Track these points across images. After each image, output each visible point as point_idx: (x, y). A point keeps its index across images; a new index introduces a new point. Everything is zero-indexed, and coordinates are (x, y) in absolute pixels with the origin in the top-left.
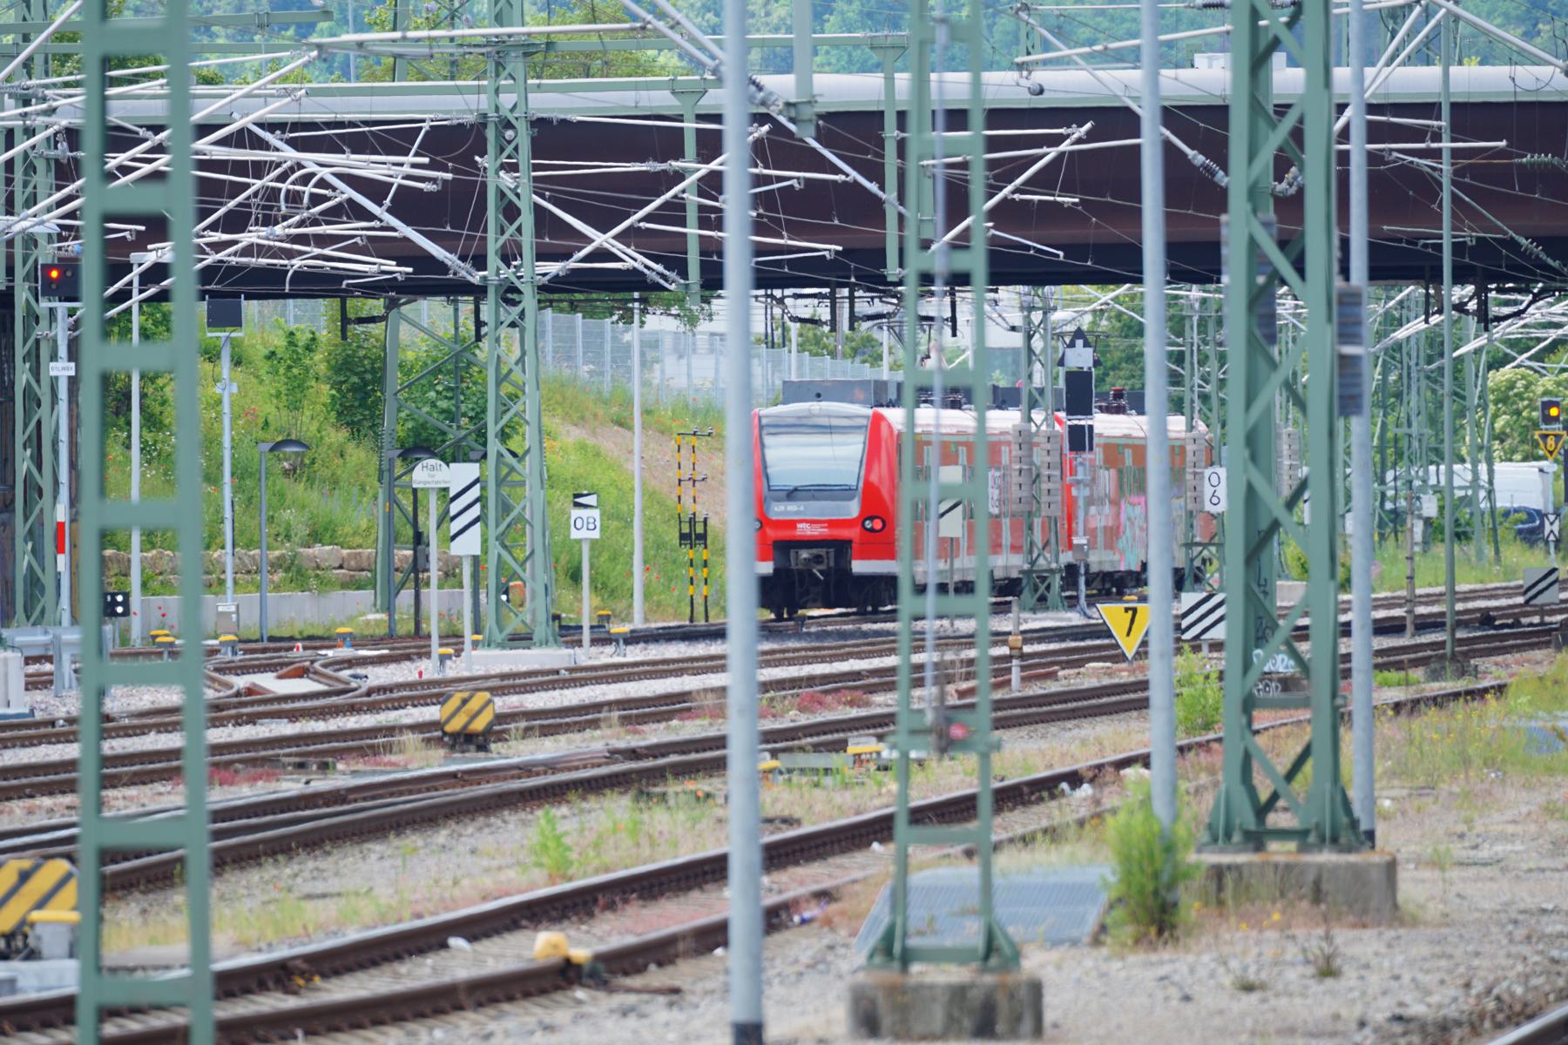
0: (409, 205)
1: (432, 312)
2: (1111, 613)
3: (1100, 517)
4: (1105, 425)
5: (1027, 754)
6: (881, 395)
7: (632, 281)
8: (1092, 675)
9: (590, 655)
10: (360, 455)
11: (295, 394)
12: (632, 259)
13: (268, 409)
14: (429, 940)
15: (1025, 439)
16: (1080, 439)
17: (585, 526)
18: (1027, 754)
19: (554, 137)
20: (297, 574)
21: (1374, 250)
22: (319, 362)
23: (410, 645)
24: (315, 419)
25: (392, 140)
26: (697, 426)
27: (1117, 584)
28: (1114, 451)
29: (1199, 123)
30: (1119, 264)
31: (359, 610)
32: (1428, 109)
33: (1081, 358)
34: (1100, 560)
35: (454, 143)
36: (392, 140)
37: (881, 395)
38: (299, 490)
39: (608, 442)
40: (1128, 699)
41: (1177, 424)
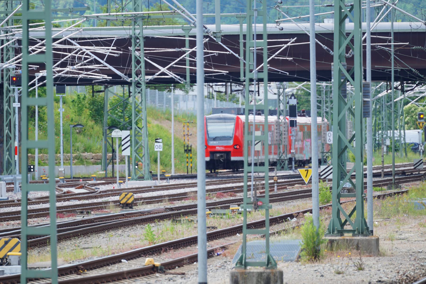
0: (111, 60)
1: (117, 89)
2: (301, 171)
3: (298, 145)
4: (300, 120)
5: (279, 209)
6: (239, 112)
7: (171, 81)
8: (297, 188)
9: (159, 183)
10: (98, 128)
11: (80, 111)
12: (171, 75)
13: (73, 116)
14: (116, 260)
15: (278, 124)
16: (293, 124)
17: (158, 147)
18: (279, 209)
19: (150, 42)
20: (81, 161)
21: (373, 72)
22: (86, 103)
23: (111, 180)
24: (85, 118)
25: (106, 43)
26: (189, 120)
27: (303, 163)
28: (302, 127)
29: (326, 38)
30: (304, 76)
31: (97, 171)
32: (387, 34)
33: (293, 102)
34: (299, 157)
35: (123, 43)
36: (106, 43)
37: (239, 112)
38: (81, 137)
39: (165, 125)
40: (306, 194)
41: (319, 119)
